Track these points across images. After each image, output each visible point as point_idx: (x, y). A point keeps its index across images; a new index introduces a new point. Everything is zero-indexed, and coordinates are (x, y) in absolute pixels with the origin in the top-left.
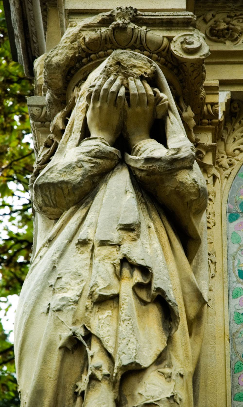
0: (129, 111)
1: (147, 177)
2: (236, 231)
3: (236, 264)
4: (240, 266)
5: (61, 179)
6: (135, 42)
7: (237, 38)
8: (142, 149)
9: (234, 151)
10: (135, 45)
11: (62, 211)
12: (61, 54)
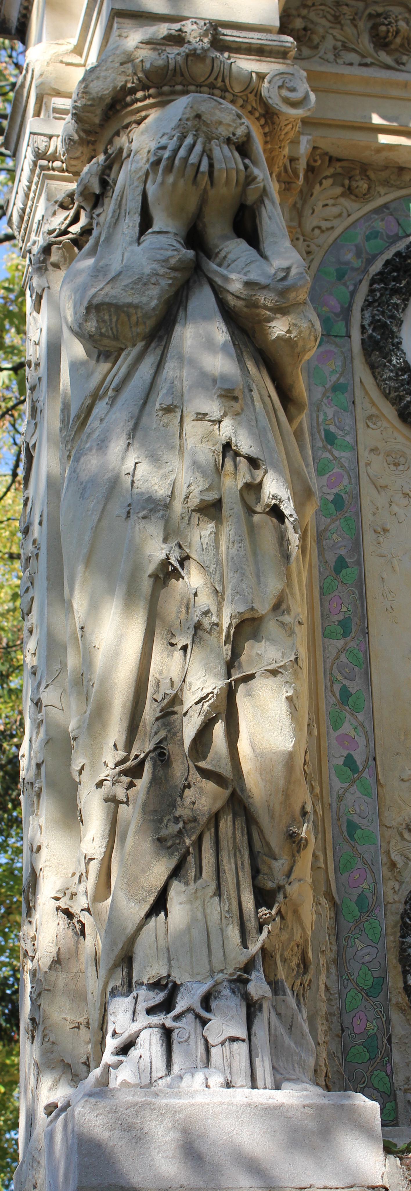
0: (212, 193)
1: (245, 310)
2: (320, 365)
3: (321, 420)
4: (327, 422)
5: (129, 300)
6: (216, 79)
7: (318, 44)
8: (231, 256)
9: (313, 230)
10: (215, 82)
11: (123, 347)
12: (105, 78)
